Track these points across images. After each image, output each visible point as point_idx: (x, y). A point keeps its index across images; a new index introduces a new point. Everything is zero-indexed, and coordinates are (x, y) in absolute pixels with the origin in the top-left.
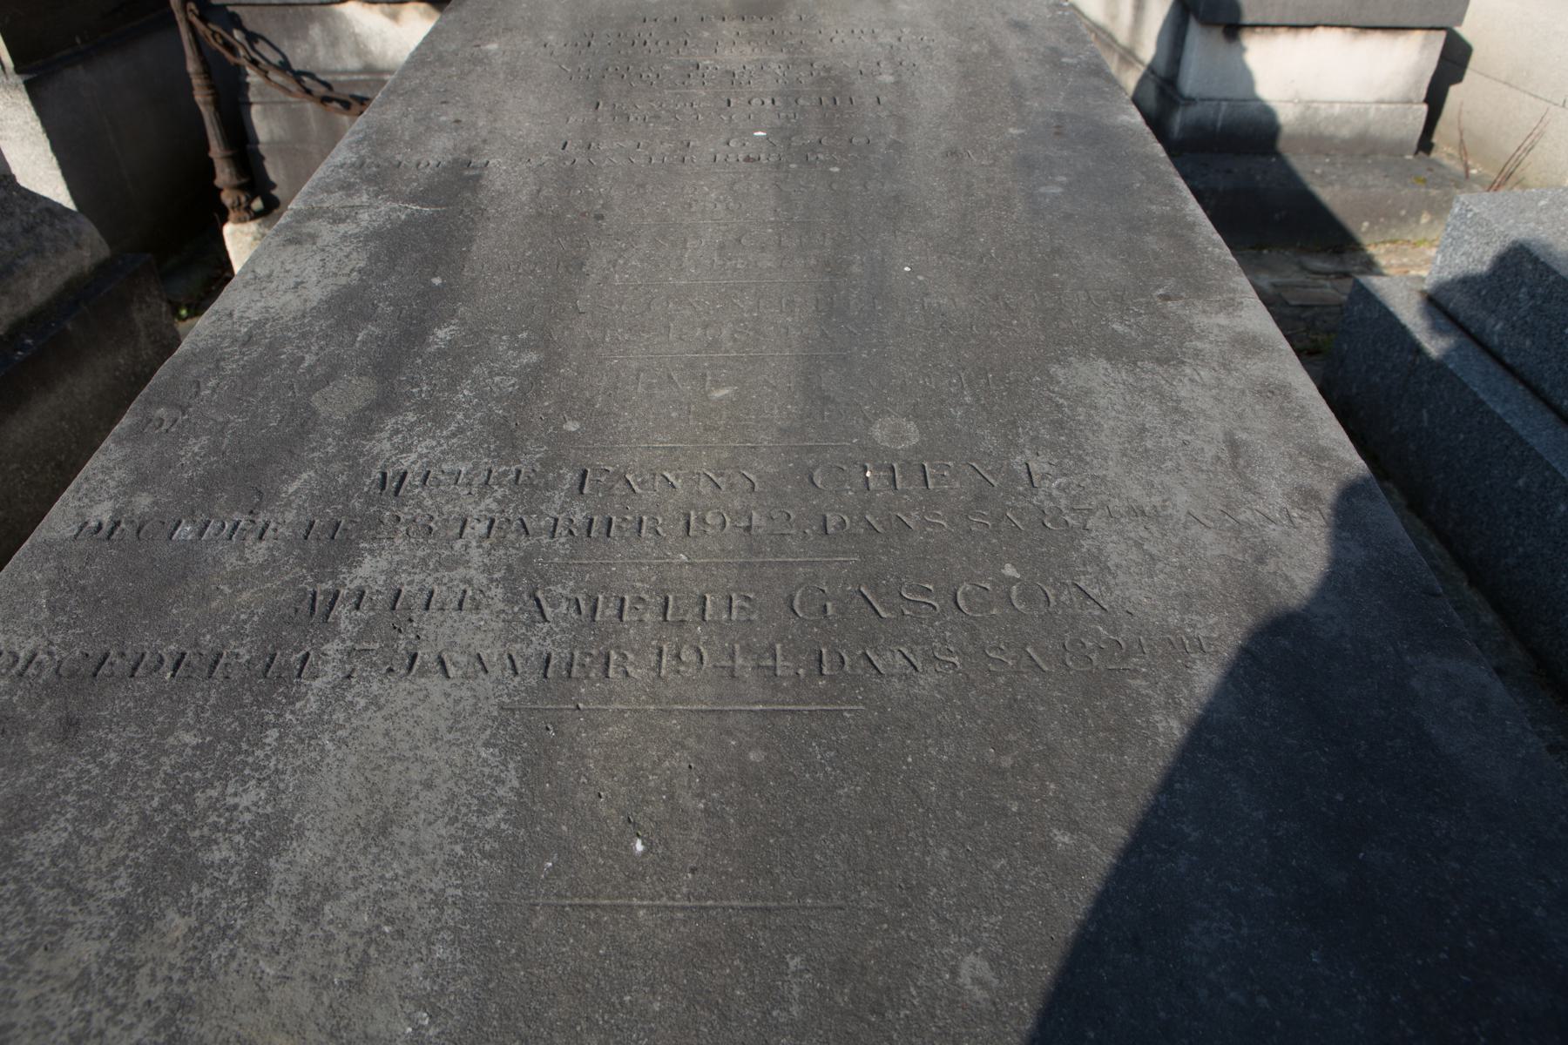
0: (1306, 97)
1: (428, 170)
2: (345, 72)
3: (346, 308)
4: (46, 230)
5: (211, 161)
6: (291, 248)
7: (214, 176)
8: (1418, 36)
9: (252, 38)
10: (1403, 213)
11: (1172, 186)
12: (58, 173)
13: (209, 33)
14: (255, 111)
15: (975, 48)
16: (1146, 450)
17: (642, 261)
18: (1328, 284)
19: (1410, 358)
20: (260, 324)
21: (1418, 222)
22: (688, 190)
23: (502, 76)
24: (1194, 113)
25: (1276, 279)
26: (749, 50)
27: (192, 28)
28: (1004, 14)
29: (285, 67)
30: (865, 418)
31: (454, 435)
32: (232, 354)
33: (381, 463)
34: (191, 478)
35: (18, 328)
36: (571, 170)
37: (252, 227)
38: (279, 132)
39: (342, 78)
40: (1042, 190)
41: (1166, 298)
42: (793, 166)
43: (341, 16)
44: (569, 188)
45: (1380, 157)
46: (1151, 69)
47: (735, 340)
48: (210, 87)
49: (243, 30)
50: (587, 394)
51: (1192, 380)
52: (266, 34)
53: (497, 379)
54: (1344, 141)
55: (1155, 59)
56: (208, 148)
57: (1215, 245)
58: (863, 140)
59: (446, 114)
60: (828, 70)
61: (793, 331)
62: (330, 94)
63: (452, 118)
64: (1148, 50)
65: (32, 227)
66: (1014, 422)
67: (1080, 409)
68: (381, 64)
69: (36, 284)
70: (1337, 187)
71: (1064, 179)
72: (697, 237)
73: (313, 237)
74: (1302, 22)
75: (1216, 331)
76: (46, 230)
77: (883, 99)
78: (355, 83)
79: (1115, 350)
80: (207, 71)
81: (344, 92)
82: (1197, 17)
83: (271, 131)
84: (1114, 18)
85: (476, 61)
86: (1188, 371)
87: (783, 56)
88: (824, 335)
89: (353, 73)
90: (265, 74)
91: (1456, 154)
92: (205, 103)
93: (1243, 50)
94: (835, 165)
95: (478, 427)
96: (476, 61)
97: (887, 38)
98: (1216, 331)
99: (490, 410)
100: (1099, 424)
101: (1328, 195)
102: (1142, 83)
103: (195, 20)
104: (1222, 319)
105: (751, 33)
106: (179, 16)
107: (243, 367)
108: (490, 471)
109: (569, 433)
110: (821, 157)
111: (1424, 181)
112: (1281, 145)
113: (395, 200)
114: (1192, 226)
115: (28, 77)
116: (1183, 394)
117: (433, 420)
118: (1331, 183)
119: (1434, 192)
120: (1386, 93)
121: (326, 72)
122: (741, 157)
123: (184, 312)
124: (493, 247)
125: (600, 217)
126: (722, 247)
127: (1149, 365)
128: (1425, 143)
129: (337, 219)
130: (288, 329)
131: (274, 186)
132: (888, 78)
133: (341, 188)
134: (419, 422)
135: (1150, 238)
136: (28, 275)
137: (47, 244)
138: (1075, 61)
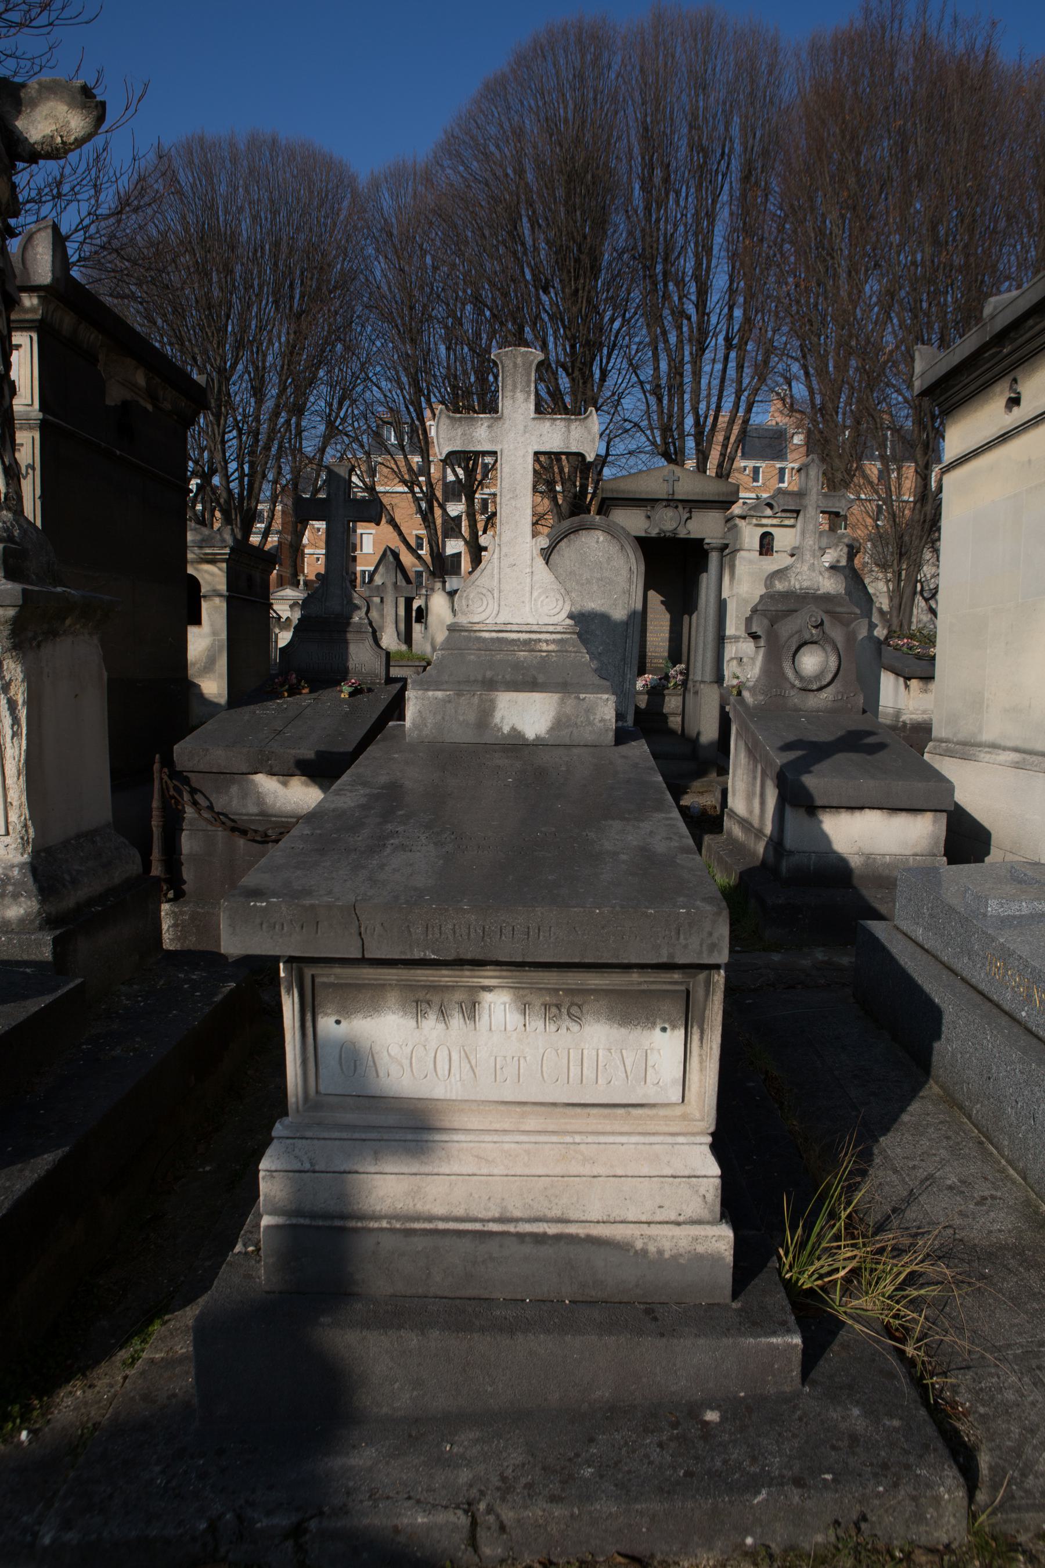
8: (929, 816)
9: (193, 791)
14: (184, 834)
29: (211, 808)
39: (245, 818)
43: (253, 780)
46: (771, 839)
50: (351, 1484)
64: (768, 829)
68: (270, 811)
74: (853, 805)
84: (751, 812)
89: (252, 815)
93: (821, 822)
106: (156, 775)
112: (856, 882)
120: (918, 850)
131: (185, 882)
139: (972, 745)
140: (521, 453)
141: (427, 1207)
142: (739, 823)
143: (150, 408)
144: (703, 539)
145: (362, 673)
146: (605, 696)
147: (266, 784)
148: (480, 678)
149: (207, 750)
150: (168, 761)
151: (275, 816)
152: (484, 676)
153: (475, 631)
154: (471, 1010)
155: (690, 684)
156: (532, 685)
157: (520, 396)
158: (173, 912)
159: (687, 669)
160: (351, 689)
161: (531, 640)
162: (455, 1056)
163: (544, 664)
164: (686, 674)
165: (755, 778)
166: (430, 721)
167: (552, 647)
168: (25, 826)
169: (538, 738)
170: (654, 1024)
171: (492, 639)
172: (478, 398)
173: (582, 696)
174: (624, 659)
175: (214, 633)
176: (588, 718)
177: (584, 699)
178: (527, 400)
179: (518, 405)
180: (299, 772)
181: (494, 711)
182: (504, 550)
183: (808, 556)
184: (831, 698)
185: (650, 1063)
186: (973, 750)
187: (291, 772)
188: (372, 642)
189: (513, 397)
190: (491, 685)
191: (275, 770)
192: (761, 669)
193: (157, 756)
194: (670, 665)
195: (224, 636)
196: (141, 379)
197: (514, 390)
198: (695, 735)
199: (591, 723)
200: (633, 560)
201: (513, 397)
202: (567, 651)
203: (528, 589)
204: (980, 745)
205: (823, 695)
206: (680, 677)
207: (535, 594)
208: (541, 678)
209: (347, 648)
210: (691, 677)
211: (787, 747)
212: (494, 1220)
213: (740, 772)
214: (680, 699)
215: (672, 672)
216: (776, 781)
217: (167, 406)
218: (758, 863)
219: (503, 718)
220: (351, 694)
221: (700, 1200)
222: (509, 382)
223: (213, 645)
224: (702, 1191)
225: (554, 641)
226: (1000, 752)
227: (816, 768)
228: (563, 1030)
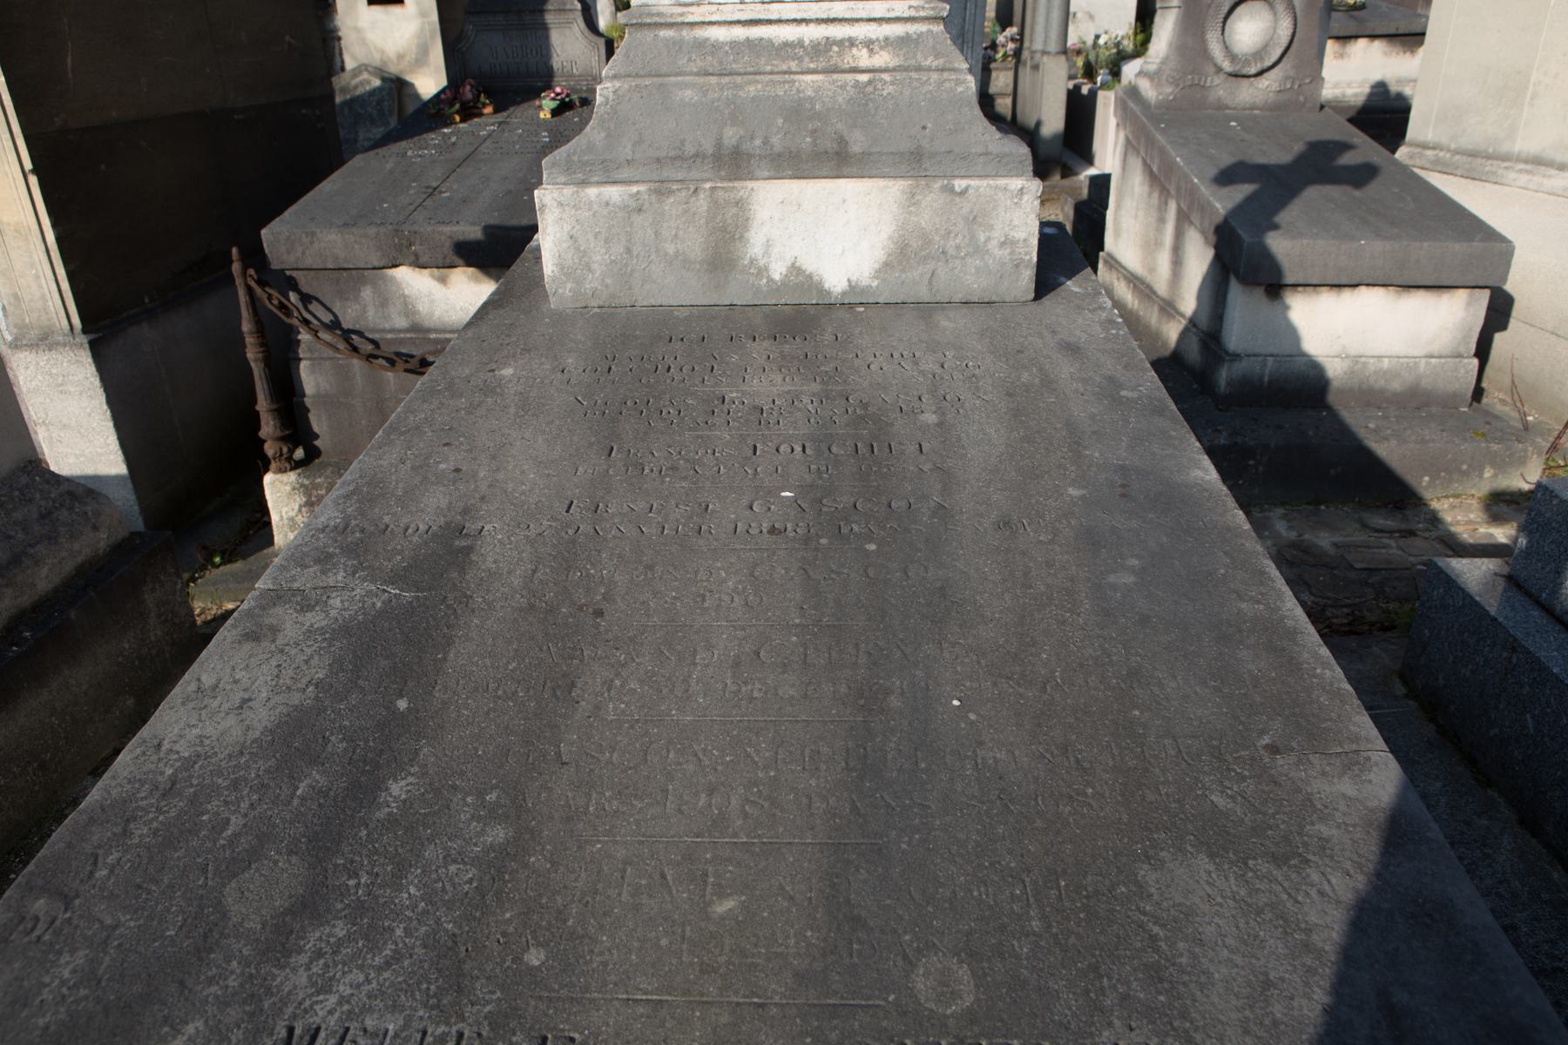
0: (1353, 352)
1: (415, 539)
2: (392, 331)
3: (293, 741)
4: (64, 514)
5: (257, 413)
6: (247, 647)
7: (258, 428)
9: (306, 299)
10: (1465, 467)
11: (1262, 573)
12: (111, 424)
13: (265, 297)
14: (303, 365)
15: (1025, 377)
16: (1276, 1023)
17: (641, 682)
18: (1392, 543)
19: (1505, 654)
20: (188, 764)
21: (1481, 476)
22: (702, 575)
23: (512, 410)
24: (1240, 368)
25: (1337, 539)
26: (779, 379)
27: (250, 290)
28: (1054, 332)
29: (335, 325)
30: (905, 957)
31: (388, 964)
32: (146, 811)
33: (289, 1010)
34: (47, 1028)
35: (19, 619)
36: (574, 542)
37: (292, 477)
38: (325, 386)
39: (389, 336)
40: (1112, 578)
41: (1274, 749)
42: (824, 541)
43: (393, 278)
44: (568, 569)
45: (1434, 409)
46: (1192, 322)
47: (746, 815)
48: (262, 345)
49: (299, 292)
51: (1321, 893)
52: (319, 296)
53: (453, 868)
54: (1395, 394)
55: (1195, 313)
56: (255, 401)
57: (1325, 665)
58: (904, 504)
59: (446, 460)
60: (865, 406)
61: (818, 804)
62: (376, 352)
63: (452, 466)
64: (1189, 304)
65: (50, 513)
66: (1095, 968)
67: (1181, 945)
68: (427, 324)
69: (44, 571)
70: (1393, 442)
71: (1134, 562)
72: (709, 647)
73: (275, 630)
75: (1342, 807)
76: (64, 514)
77: (925, 447)
78: (402, 342)
79: (1220, 840)
80: (260, 330)
81: (388, 350)
82: (1237, 277)
83: (318, 385)
84: (1152, 270)
85: (488, 390)
86: (1315, 877)
87: (815, 387)
88: (854, 809)
89: (400, 331)
90: (315, 333)
91: (1509, 400)
92: (256, 360)
93: (1287, 308)
94: (871, 540)
95: (419, 951)
96: (488, 390)
97: (929, 364)
98: (1342, 807)
99: (438, 922)
100: (1206, 972)
101: (1385, 450)
102: (1183, 335)
103: (253, 284)
104: (1347, 787)
105: (783, 357)
106: (239, 281)
107: (155, 832)
108: (425, 1033)
109: (531, 969)
110: (856, 528)
111: (1484, 435)
112: (1331, 398)
113: (374, 581)
114: (1292, 634)
115: (92, 336)
116: (1313, 918)
117: (366, 938)
118: (1386, 439)
119: (1495, 447)
120: (1435, 348)
121: (374, 330)
122: (765, 526)
123: (217, 560)
124: (476, 653)
125: (599, 613)
126: (737, 664)
127: (1264, 866)
128: (1478, 393)
129: (306, 607)
130: (220, 773)
131: (317, 437)
132: (930, 418)
133: (318, 561)
134: (349, 938)
135: (1244, 654)
136: (37, 563)
137: (62, 530)
138: (1135, 395)
139: (1489, 157)
145: (573, 75)
146: (1016, 183)
147: (413, 282)
148: (708, 147)
149: (313, 234)
150: (255, 256)
151: (436, 331)
152: (719, 144)
153: (692, 25)
154: (795, 269)
155: (1025, 54)
156: (836, 160)
158: (302, 485)
159: (1021, 33)
160: (553, 104)
161: (829, 42)
163: (863, 104)
164: (1020, 39)
165: (1162, 220)
166: (599, 258)
167: (882, 59)
169: (853, 288)
171: (734, 44)
173: (959, 184)
175: (423, 14)
176: (973, 237)
177: (964, 192)
180: (460, 261)
181: (746, 228)
184: (1275, 87)
186: (1489, 166)
187: (448, 262)
188: (582, 25)
190: (735, 163)
191: (422, 260)
192: (1170, 45)
193: (234, 250)
194: (998, 28)
195: (435, 17)
198: (1032, 125)
199: (979, 250)
202: (919, 69)
204: (1506, 158)
205: (1264, 82)
206: (1011, 46)
208: (858, 143)
209: (547, 37)
210: (1026, 44)
211: (1226, 177)
213: (1129, 205)
214: (1011, 74)
215: (1001, 39)
216: (1213, 238)
218: (1167, 353)
219: (768, 244)
220: (555, 112)
223: (422, 30)
225: (887, 43)
226: (1553, 172)
227: (1282, 217)
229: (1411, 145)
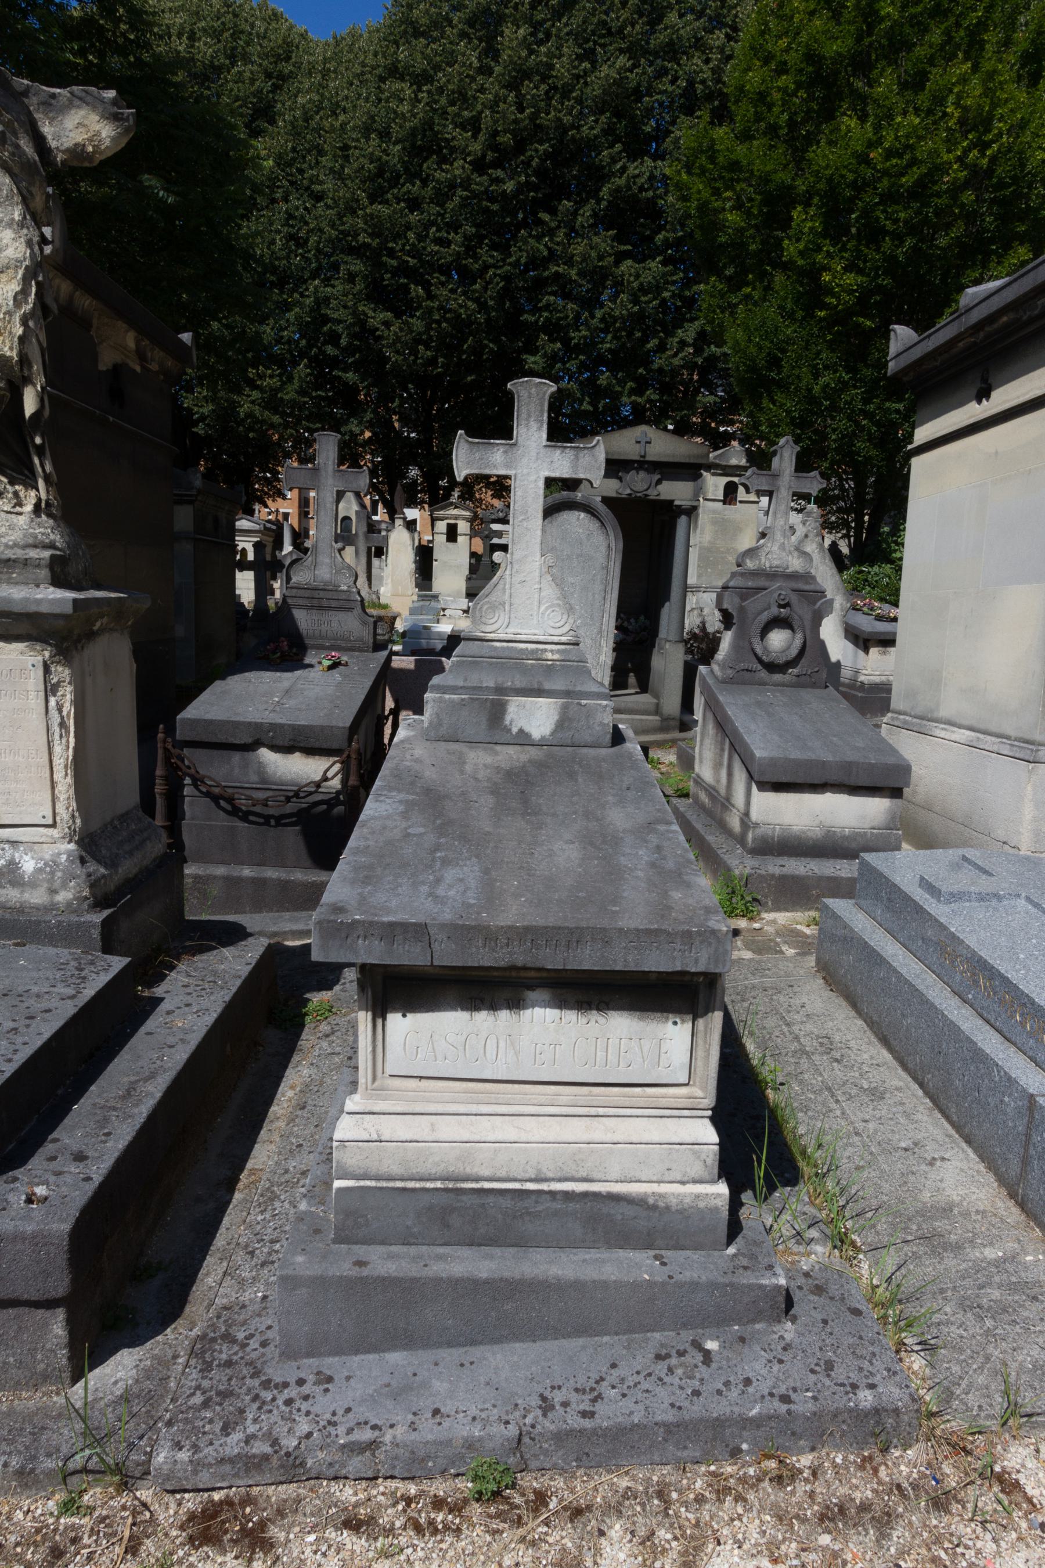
24: (759, 832)
120: (875, 824)
140: (533, 478)
141: (475, 1170)
142: (706, 790)
143: (138, 369)
144: (672, 501)
157: (534, 425)
161: (537, 650)
162: (502, 1044)
165: (722, 750)
167: (556, 657)
168: (73, 816)
169: (543, 738)
170: (667, 1019)
172: (497, 426)
174: (600, 632)
178: (540, 429)
179: (531, 431)
182: (516, 567)
183: (778, 536)
185: (663, 1050)
189: (527, 425)
196: (130, 340)
197: (527, 419)
200: (612, 537)
201: (527, 425)
203: (536, 603)
207: (543, 608)
212: (531, 1180)
217: (154, 367)
221: (702, 1164)
222: (524, 410)
224: (703, 1156)
225: (558, 651)
228: (593, 1022)
229: (894, 712)
